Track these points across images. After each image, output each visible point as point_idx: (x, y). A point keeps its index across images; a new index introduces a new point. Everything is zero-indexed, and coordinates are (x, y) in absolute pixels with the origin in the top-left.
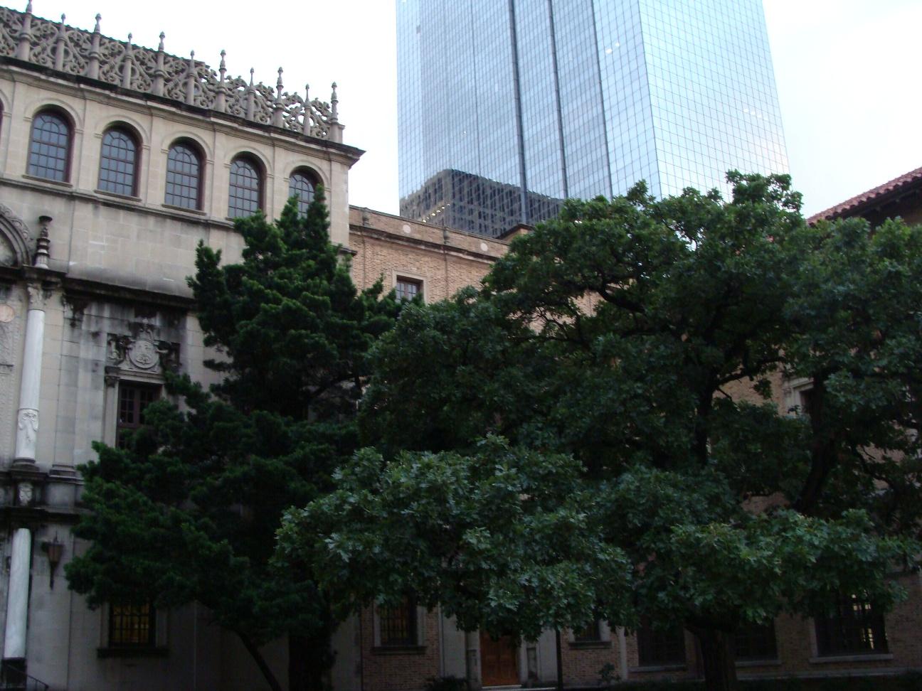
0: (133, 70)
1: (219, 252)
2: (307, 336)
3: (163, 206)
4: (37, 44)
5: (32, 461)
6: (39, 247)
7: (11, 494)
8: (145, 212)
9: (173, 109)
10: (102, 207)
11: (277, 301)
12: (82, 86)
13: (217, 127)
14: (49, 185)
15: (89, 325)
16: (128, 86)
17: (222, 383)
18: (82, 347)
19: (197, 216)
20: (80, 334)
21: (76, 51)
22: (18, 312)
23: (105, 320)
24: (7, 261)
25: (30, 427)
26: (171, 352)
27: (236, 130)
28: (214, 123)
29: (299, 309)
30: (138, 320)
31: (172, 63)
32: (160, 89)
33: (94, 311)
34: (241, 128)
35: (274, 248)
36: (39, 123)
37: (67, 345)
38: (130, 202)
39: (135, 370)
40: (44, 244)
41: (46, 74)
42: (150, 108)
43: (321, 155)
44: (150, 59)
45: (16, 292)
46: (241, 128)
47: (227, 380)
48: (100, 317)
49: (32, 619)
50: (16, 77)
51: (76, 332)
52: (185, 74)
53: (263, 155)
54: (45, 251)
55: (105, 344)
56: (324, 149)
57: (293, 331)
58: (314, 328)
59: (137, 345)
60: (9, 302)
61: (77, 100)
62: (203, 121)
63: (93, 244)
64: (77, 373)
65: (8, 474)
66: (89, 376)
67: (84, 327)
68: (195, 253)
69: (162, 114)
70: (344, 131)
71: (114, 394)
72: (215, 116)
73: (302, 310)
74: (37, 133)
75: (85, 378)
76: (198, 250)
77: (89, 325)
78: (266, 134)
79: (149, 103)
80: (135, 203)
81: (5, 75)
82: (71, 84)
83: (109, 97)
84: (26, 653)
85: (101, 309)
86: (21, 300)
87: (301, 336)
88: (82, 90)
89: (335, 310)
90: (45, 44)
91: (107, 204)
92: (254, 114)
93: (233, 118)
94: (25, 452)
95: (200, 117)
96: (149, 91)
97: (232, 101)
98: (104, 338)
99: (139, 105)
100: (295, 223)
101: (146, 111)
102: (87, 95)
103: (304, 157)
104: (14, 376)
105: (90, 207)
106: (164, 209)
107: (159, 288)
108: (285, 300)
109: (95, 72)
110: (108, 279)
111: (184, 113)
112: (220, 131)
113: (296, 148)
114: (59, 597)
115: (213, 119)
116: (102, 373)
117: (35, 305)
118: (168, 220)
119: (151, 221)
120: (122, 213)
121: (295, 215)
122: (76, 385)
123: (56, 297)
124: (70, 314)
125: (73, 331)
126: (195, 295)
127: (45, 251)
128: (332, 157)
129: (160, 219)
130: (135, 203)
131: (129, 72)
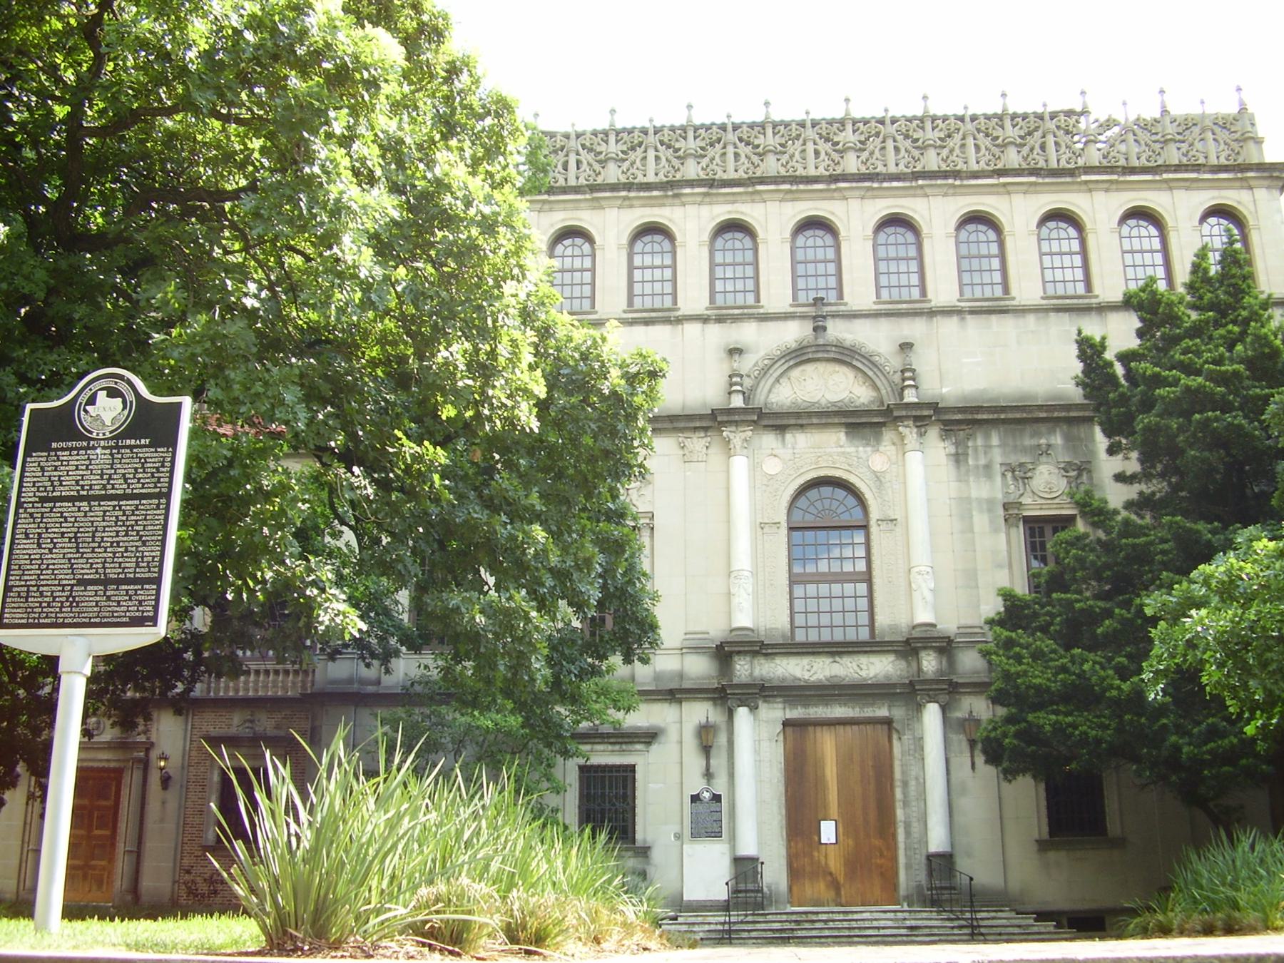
0: (1056, 144)
1: (1104, 338)
2: (1217, 419)
3: (1043, 298)
4: (624, 160)
5: (934, 625)
6: (904, 380)
7: (914, 665)
8: (1022, 311)
9: (1033, 179)
10: (968, 317)
11: (1176, 382)
12: (920, 182)
13: (1091, 186)
14: (904, 306)
15: (976, 459)
16: (975, 167)
17: (1135, 496)
18: (972, 485)
19: (1086, 301)
20: (968, 471)
21: (908, 143)
22: (894, 458)
23: (993, 448)
24: (872, 402)
25: (924, 585)
26: (1081, 469)
27: (1117, 182)
28: (1086, 182)
29: (1200, 386)
30: (1034, 442)
31: (1021, 123)
32: (1012, 158)
33: (980, 442)
34: (1122, 179)
35: (1173, 319)
36: (1125, 230)
37: (954, 485)
38: (1002, 303)
39: (1040, 501)
40: (908, 374)
41: (878, 181)
42: (1166, 181)
43: (1238, 184)
44: (989, 126)
45: (888, 435)
46: (1122, 179)
47: (1141, 493)
48: (988, 447)
49: (954, 806)
50: (847, 194)
51: (963, 469)
52: (801, 140)
53: (1160, 205)
54: (912, 383)
55: (998, 479)
56: (1239, 175)
57: (1197, 416)
58: (1226, 407)
59: (1037, 472)
60: (882, 448)
61: (1081, 195)
62: (1073, 183)
63: (964, 362)
64: (971, 517)
65: (907, 642)
66: (985, 517)
67: (971, 462)
68: (1075, 346)
69: (1183, 184)
70: (1264, 145)
71: (1019, 534)
72: (1086, 173)
73: (1205, 386)
74: (964, 247)
75: (981, 521)
76: (1077, 342)
77: (976, 459)
78: (1157, 178)
79: (1002, 180)
80: (1007, 303)
81: (836, 195)
82: (907, 184)
83: (954, 186)
84: (952, 845)
85: (987, 437)
86: (894, 444)
87: (1208, 419)
88: (922, 187)
89: (1254, 378)
90: (792, 150)
91: (973, 312)
92: (1134, 153)
93: (1110, 170)
94: (924, 616)
95: (1068, 179)
96: (1000, 166)
97: (1184, 147)
98: (997, 469)
99: (992, 185)
100: (1207, 280)
101: (1002, 190)
102: (928, 191)
103: (1215, 193)
104: (899, 530)
105: (955, 319)
106: (1044, 302)
107: (1054, 399)
108: (1185, 380)
109: (932, 161)
110: (990, 400)
111: (1047, 180)
112: (1096, 190)
113: (1200, 184)
114: (981, 778)
115: (1084, 178)
116: (1001, 512)
117: (908, 447)
118: (1052, 314)
119: (1031, 318)
120: (994, 318)
121: (1206, 271)
122: (971, 530)
123: (933, 433)
124: (952, 449)
125: (958, 468)
126: (1086, 397)
127: (912, 383)
128: (1252, 183)
129: (1041, 315)
130: (1007, 303)
131: (973, 150)
